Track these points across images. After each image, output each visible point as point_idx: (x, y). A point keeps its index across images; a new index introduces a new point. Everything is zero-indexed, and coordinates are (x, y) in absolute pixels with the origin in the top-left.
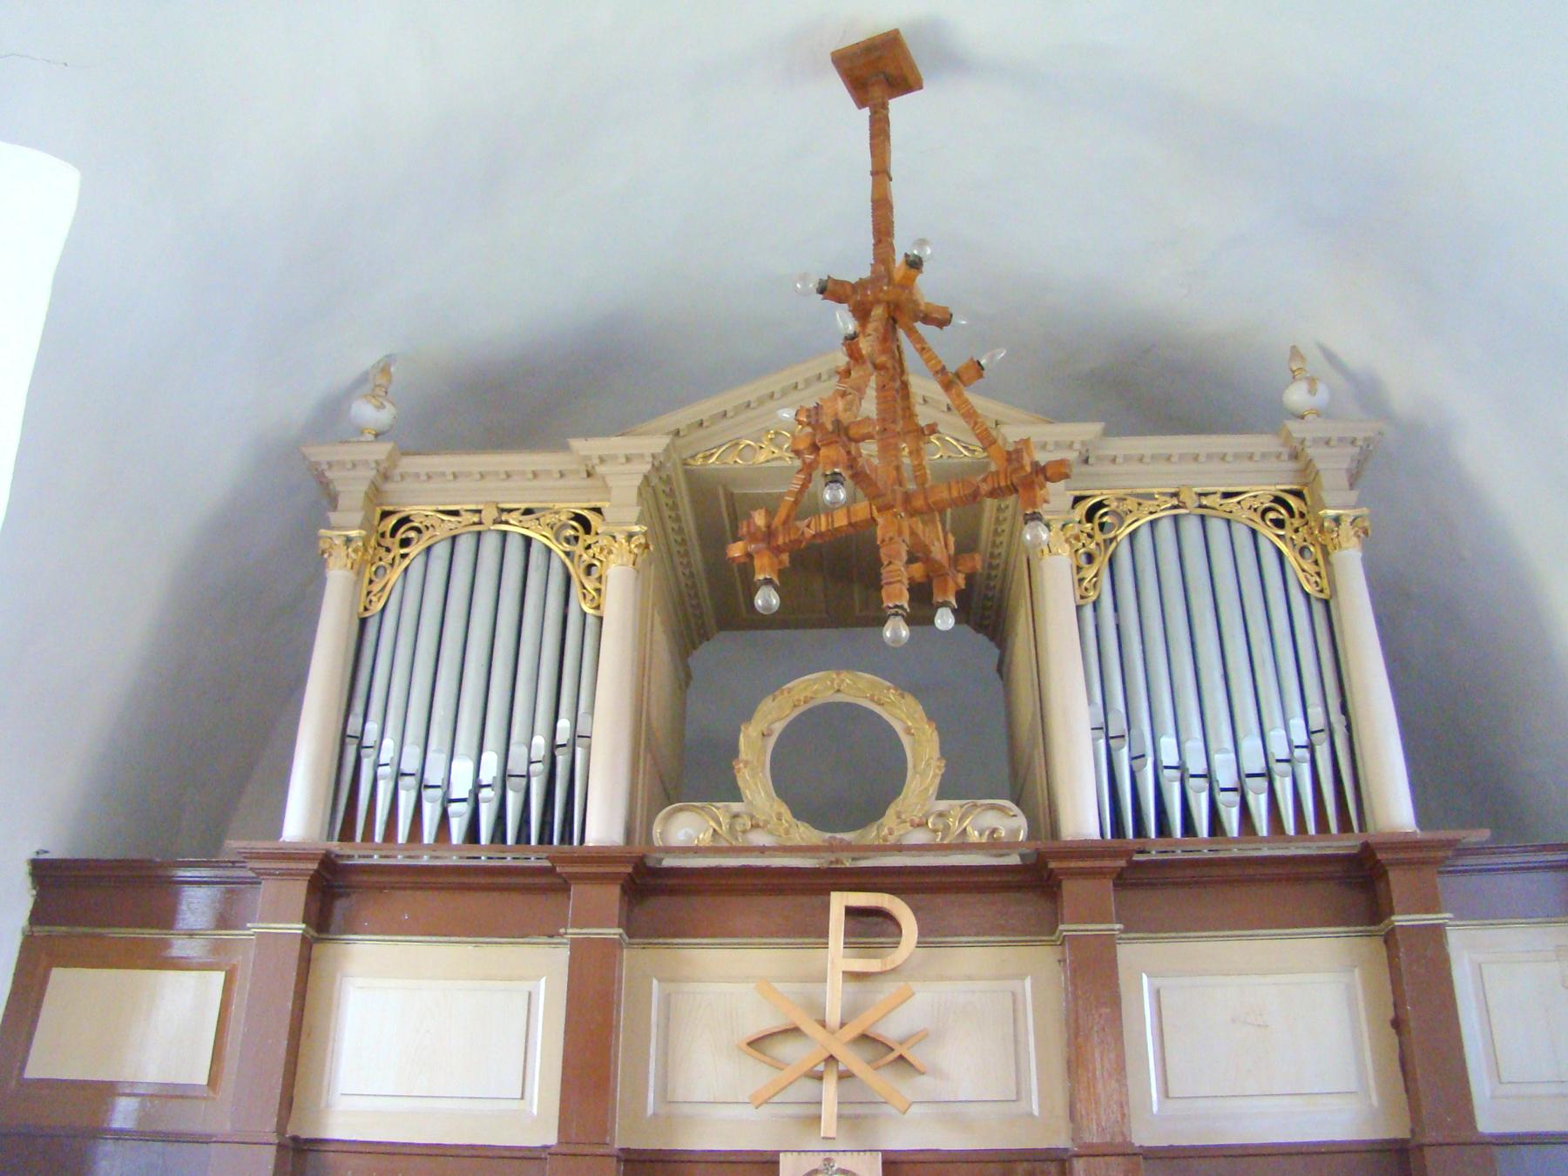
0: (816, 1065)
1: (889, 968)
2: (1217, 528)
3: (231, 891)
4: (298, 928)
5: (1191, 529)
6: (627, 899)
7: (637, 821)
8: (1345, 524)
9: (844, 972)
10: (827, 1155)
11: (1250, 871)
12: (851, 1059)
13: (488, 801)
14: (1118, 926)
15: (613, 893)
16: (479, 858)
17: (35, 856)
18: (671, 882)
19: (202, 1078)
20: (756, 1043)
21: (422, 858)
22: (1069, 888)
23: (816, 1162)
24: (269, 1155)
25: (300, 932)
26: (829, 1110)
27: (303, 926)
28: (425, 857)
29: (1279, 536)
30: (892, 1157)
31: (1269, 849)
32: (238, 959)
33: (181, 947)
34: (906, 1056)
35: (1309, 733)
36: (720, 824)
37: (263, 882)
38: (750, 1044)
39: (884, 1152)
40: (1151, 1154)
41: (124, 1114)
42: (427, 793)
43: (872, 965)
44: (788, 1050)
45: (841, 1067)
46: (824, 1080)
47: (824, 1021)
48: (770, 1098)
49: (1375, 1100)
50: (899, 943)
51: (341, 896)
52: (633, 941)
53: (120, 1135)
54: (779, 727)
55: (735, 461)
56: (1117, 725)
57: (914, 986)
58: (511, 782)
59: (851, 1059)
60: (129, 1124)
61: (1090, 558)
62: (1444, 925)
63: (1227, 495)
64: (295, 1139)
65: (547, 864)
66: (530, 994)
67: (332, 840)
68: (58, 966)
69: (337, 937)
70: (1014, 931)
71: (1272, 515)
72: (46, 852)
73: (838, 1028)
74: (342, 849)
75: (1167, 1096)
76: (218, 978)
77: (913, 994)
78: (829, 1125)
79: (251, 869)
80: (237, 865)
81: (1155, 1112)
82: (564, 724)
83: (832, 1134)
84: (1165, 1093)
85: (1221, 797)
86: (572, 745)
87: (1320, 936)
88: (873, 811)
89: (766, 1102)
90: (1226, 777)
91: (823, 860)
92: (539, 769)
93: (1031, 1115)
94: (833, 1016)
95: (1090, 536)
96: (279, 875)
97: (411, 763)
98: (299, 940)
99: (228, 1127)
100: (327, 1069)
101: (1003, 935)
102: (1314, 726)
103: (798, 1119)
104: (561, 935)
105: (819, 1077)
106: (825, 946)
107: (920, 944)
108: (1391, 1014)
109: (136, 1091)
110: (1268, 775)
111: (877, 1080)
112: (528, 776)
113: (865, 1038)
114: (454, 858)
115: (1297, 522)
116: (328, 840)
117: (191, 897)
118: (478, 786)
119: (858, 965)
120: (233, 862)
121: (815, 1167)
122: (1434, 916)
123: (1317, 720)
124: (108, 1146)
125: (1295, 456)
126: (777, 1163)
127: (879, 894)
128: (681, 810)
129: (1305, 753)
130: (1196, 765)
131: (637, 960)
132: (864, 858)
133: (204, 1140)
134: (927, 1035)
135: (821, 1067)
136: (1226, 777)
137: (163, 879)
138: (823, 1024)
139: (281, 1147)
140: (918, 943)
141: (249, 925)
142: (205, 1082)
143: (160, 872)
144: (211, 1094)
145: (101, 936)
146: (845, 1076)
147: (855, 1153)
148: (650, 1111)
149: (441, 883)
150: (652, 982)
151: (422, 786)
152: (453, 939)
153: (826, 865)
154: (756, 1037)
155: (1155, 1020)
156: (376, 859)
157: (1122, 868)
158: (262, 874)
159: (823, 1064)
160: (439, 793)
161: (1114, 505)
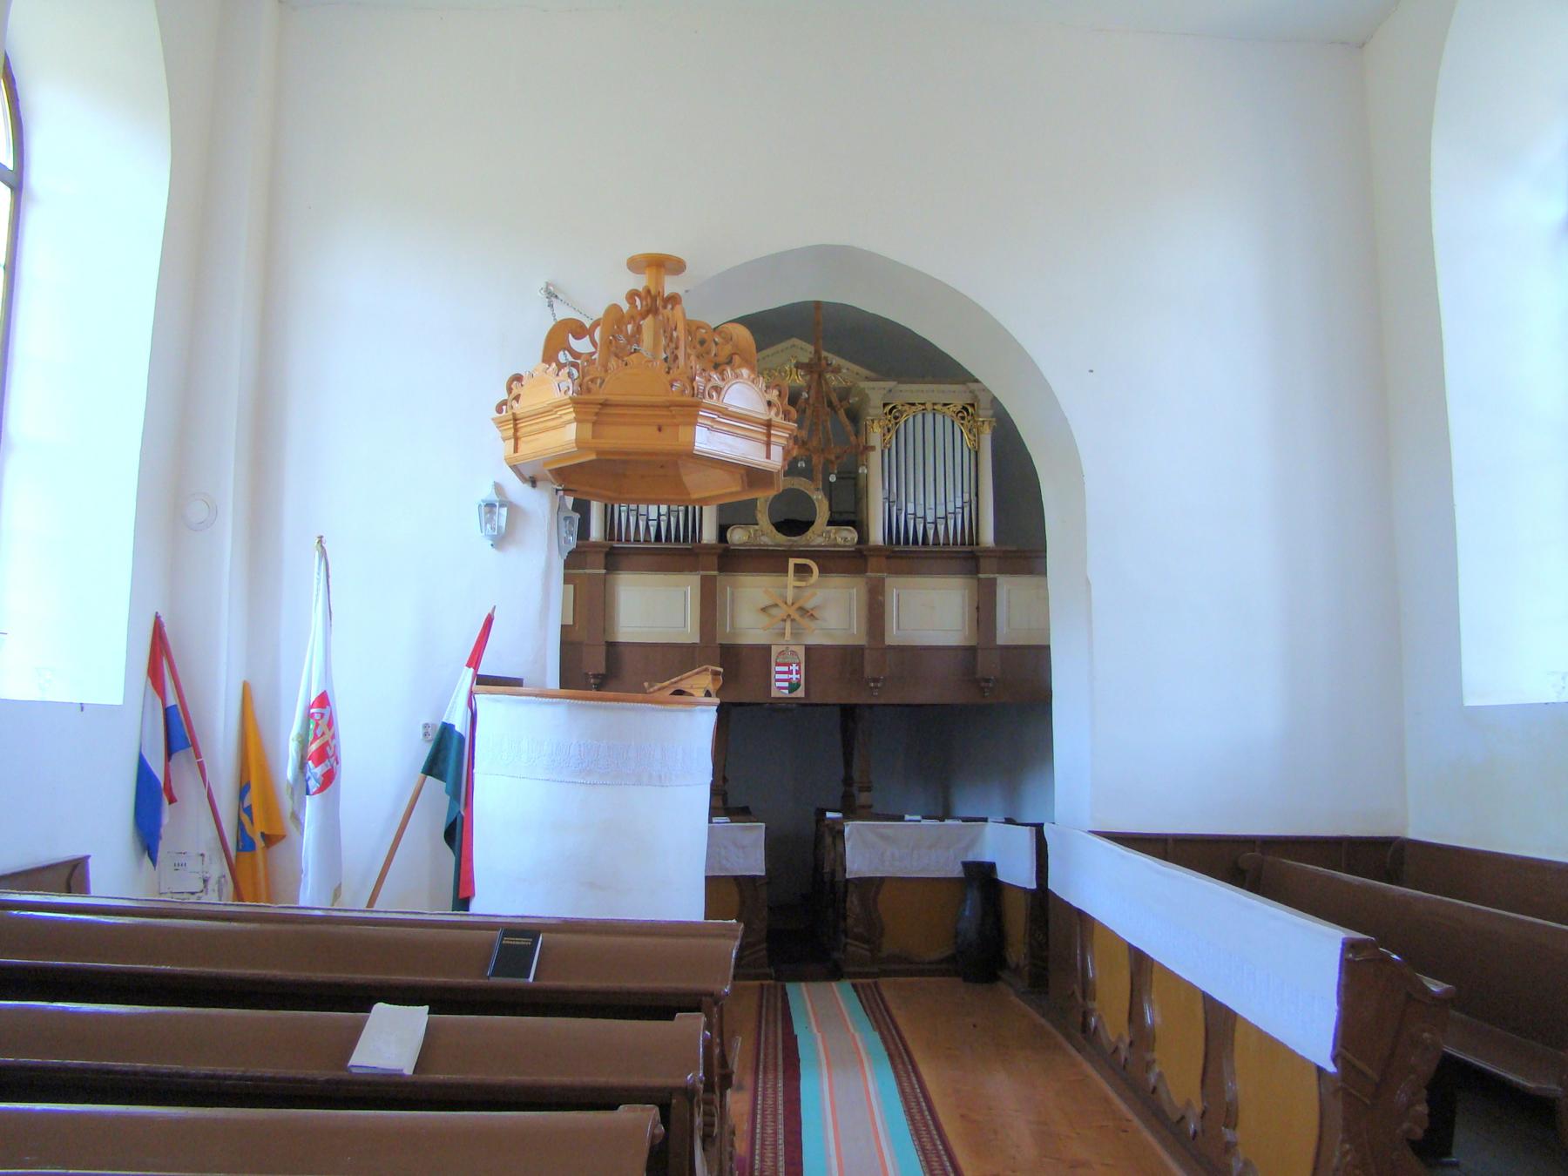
2: (939, 418)
5: (929, 417)
8: (986, 423)
12: (796, 616)
20: (764, 610)
23: (784, 648)
29: (962, 424)
30: (784, 572)
35: (963, 502)
42: (640, 518)
43: (803, 584)
44: (774, 611)
56: (893, 497)
61: (889, 430)
63: (945, 405)
71: (960, 415)
84: (898, 628)
85: (928, 525)
90: (930, 518)
94: (789, 601)
95: (889, 421)
102: (965, 500)
105: (784, 620)
108: (976, 605)
110: (946, 518)
111: (805, 622)
112: (678, 511)
115: (969, 418)
118: (659, 515)
123: (966, 498)
125: (970, 392)
129: (960, 510)
130: (920, 513)
131: (722, 579)
136: (930, 518)
146: (793, 620)
161: (900, 408)
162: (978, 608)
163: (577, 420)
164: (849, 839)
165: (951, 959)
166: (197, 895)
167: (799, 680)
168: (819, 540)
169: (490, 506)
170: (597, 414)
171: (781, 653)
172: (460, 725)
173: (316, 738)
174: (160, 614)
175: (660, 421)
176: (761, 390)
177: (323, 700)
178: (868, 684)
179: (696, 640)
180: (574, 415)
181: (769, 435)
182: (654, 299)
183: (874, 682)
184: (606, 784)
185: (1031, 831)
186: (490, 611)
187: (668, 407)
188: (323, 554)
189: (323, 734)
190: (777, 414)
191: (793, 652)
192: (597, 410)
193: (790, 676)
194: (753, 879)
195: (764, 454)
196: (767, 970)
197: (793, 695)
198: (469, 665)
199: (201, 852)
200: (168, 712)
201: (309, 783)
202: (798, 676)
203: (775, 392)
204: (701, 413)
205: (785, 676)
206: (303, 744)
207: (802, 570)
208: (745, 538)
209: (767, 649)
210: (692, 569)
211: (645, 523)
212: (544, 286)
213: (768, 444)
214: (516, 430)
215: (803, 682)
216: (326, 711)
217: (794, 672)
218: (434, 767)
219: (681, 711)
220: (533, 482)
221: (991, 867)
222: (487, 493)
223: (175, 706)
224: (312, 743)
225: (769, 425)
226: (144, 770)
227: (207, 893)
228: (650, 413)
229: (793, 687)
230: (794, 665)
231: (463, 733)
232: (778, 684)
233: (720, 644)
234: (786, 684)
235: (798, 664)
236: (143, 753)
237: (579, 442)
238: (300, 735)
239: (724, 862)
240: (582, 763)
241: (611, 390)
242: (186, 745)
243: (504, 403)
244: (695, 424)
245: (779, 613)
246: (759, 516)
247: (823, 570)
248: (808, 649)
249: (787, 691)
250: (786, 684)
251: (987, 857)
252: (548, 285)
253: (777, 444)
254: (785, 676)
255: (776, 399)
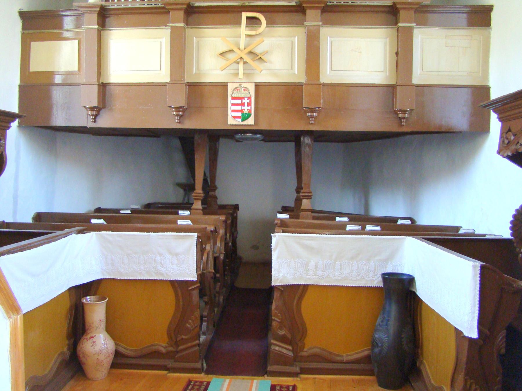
0: (237, 60)
1: (257, 34)
3: (77, 17)
4: (96, 27)
6: (186, 15)
9: (245, 35)
10: (240, 83)
11: (361, 9)
12: (247, 58)
14: (321, 23)
15: (182, 13)
16: (145, 5)
17: (19, 11)
18: (197, 10)
19: (76, 69)
21: (129, 5)
22: (308, 12)
23: (237, 85)
24: (96, 87)
25: (97, 28)
26: (241, 72)
27: (98, 26)
28: (130, 5)
31: (369, 3)
32: (81, 37)
33: (66, 34)
37: (85, 14)
38: (220, 54)
40: (324, 85)
41: (58, 79)
43: (253, 33)
44: (231, 56)
45: (244, 60)
46: (240, 64)
47: (240, 48)
48: (225, 68)
49: (388, 74)
50: (261, 27)
51: (108, 17)
52: (188, 27)
53: (57, 84)
57: (264, 38)
59: (247, 58)
60: (60, 82)
62: (413, 27)
64: (102, 83)
65: (163, 6)
66: (161, 42)
67: (103, 1)
68: (33, 41)
69: (108, 29)
70: (293, 24)
72: (22, 9)
73: (243, 49)
74: (105, 4)
75: (332, 70)
76: (76, 42)
77: (264, 41)
78: (241, 75)
79: (81, 11)
80: (77, 10)
81: (328, 74)
83: (242, 78)
84: (331, 69)
87: (379, 28)
89: (224, 70)
91: (240, 3)
93: (295, 74)
94: (242, 47)
96: (89, 12)
98: (97, 30)
99: (85, 81)
100: (109, 65)
101: (291, 25)
103: (233, 74)
104: (168, 26)
105: (238, 63)
106: (240, 27)
107: (266, 27)
108: (396, 51)
109: (60, 73)
113: (251, 53)
114: (138, 5)
116: (102, 1)
117: (66, 20)
120: (76, 9)
121: (237, 86)
122: (411, 24)
124: (55, 88)
127: (256, 13)
131: (190, 32)
132: (253, 3)
133: (79, 85)
134: (268, 52)
135: (239, 60)
137: (56, 16)
138: (239, 49)
139: (98, 85)
140: (266, 27)
141: (83, 27)
142: (77, 70)
143: (56, 13)
144: (79, 73)
145: (43, 32)
146: (245, 63)
147: (248, 83)
148: (194, 72)
150: (194, 38)
152: (139, 28)
153: (241, 5)
154: (221, 53)
155: (330, 59)
156: (116, 6)
157: (323, 7)
158: (85, 12)
159: (239, 59)
162: (397, 54)
164: (275, 249)
165: (368, 359)
171: (236, 89)
178: (306, 113)
179: (167, 79)
183: (310, 112)
185: (474, 267)
191: (246, 89)
193: (243, 108)
196: (198, 365)
197: (245, 123)
199: (511, 128)
205: (239, 108)
207: (253, 21)
209: (225, 86)
217: (246, 104)
221: (411, 280)
230: (246, 99)
234: (240, 114)
235: (249, 98)
239: (159, 267)
245: (232, 57)
247: (271, 23)
248: (258, 86)
249: (240, 120)
250: (240, 114)
251: (406, 270)
254: (239, 108)
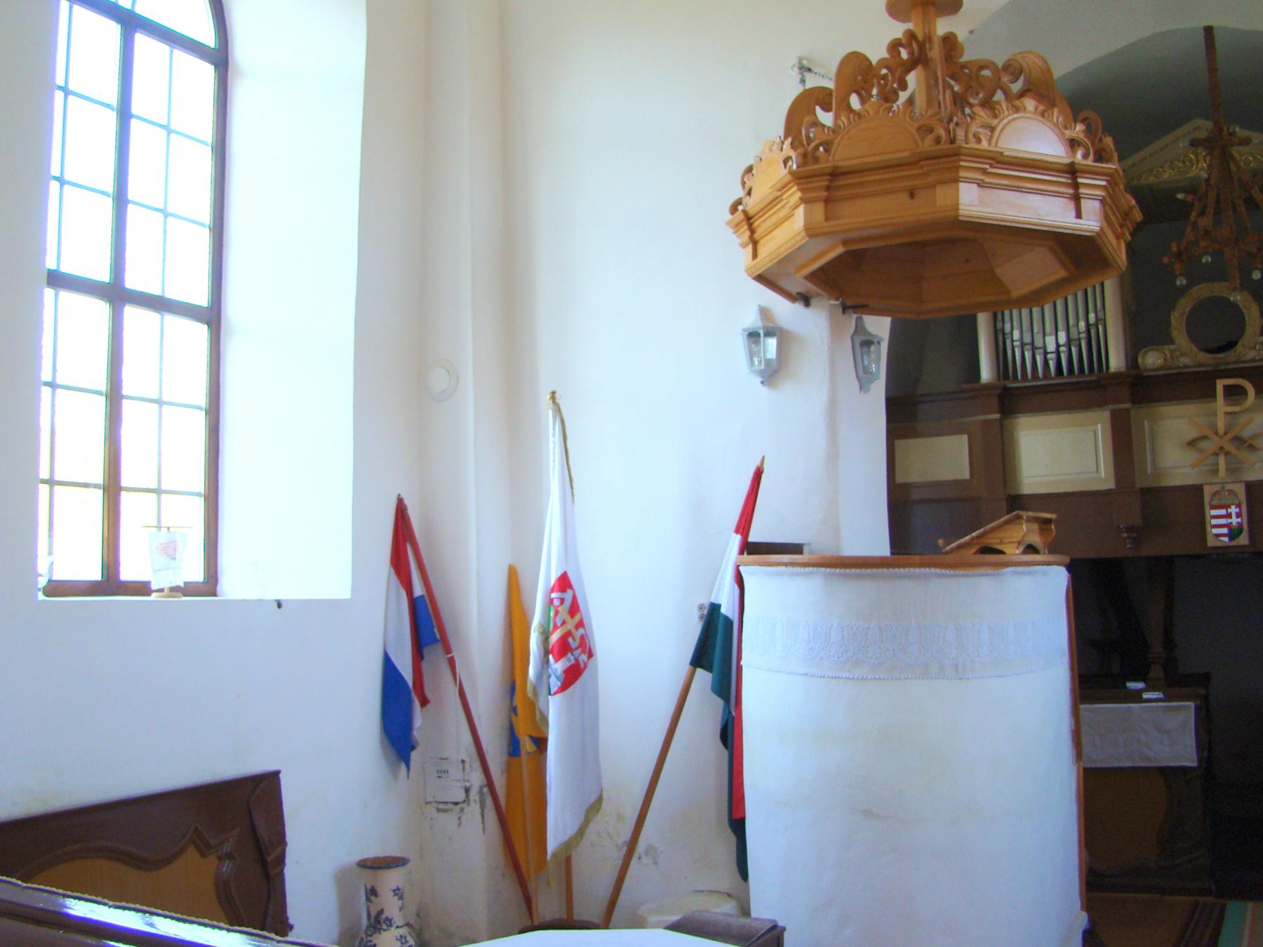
7: (1132, 361)
12: (1229, 447)
13: (1063, 352)
20: (1191, 444)
34: (1253, 444)
36: (1166, 356)
39: (1245, 482)
42: (1037, 351)
43: (1237, 409)
44: (1203, 445)
54: (1188, 310)
55: (1152, 179)
58: (1073, 342)
59: (1229, 447)
82: (1092, 316)
86: (1096, 324)
88: (1231, 345)
92: (1083, 335)
94: (1221, 429)
97: (1027, 339)
105: (1216, 454)
106: (1216, 401)
111: (1243, 454)
118: (1058, 346)
119: (1230, 409)
126: (1203, 489)
128: (1148, 351)
131: (1136, 413)
135: (1218, 451)
146: (1227, 454)
149: (1103, 242)
151: (1034, 349)
160: (1042, 351)
163: (804, 200)
166: (460, 806)
167: (1240, 525)
168: (1252, 354)
169: (753, 336)
170: (828, 188)
171: (1216, 493)
172: (728, 609)
173: (556, 627)
174: (403, 496)
175: (909, 183)
176: (1056, 125)
177: (564, 583)
180: (799, 194)
181: (1076, 186)
182: (922, 46)
184: (879, 679)
186: (758, 463)
187: (915, 163)
188: (558, 410)
189: (564, 623)
190: (1085, 156)
191: (1231, 492)
192: (825, 183)
193: (1229, 521)
194: (1184, 770)
195: (1073, 213)
197: (1235, 543)
198: (737, 531)
200: (414, 603)
201: (551, 680)
202: (1239, 520)
203: (1080, 127)
204: (962, 163)
205: (1223, 521)
206: (545, 636)
207: (1234, 393)
208: (1160, 362)
210: (1100, 404)
211: (1042, 357)
212: (795, 61)
213: (1076, 199)
214: (752, 231)
215: (1245, 526)
216: (568, 596)
217: (1234, 515)
218: (701, 659)
219: (983, 575)
220: (806, 300)
222: (751, 319)
223: (422, 597)
224: (552, 634)
225: (1072, 171)
226: (389, 670)
227: (469, 805)
228: (887, 176)
229: (1234, 533)
231: (731, 617)
232: (1215, 531)
233: (1142, 489)
234: (1225, 530)
235: (1238, 506)
236: (388, 652)
237: (811, 231)
238: (541, 625)
240: (847, 652)
241: (844, 155)
242: (435, 641)
243: (739, 202)
244: (956, 180)
246: (1175, 333)
249: (1226, 539)
250: (1225, 530)
252: (800, 60)
253: (1091, 197)
254: (1223, 521)
255: (1082, 136)
